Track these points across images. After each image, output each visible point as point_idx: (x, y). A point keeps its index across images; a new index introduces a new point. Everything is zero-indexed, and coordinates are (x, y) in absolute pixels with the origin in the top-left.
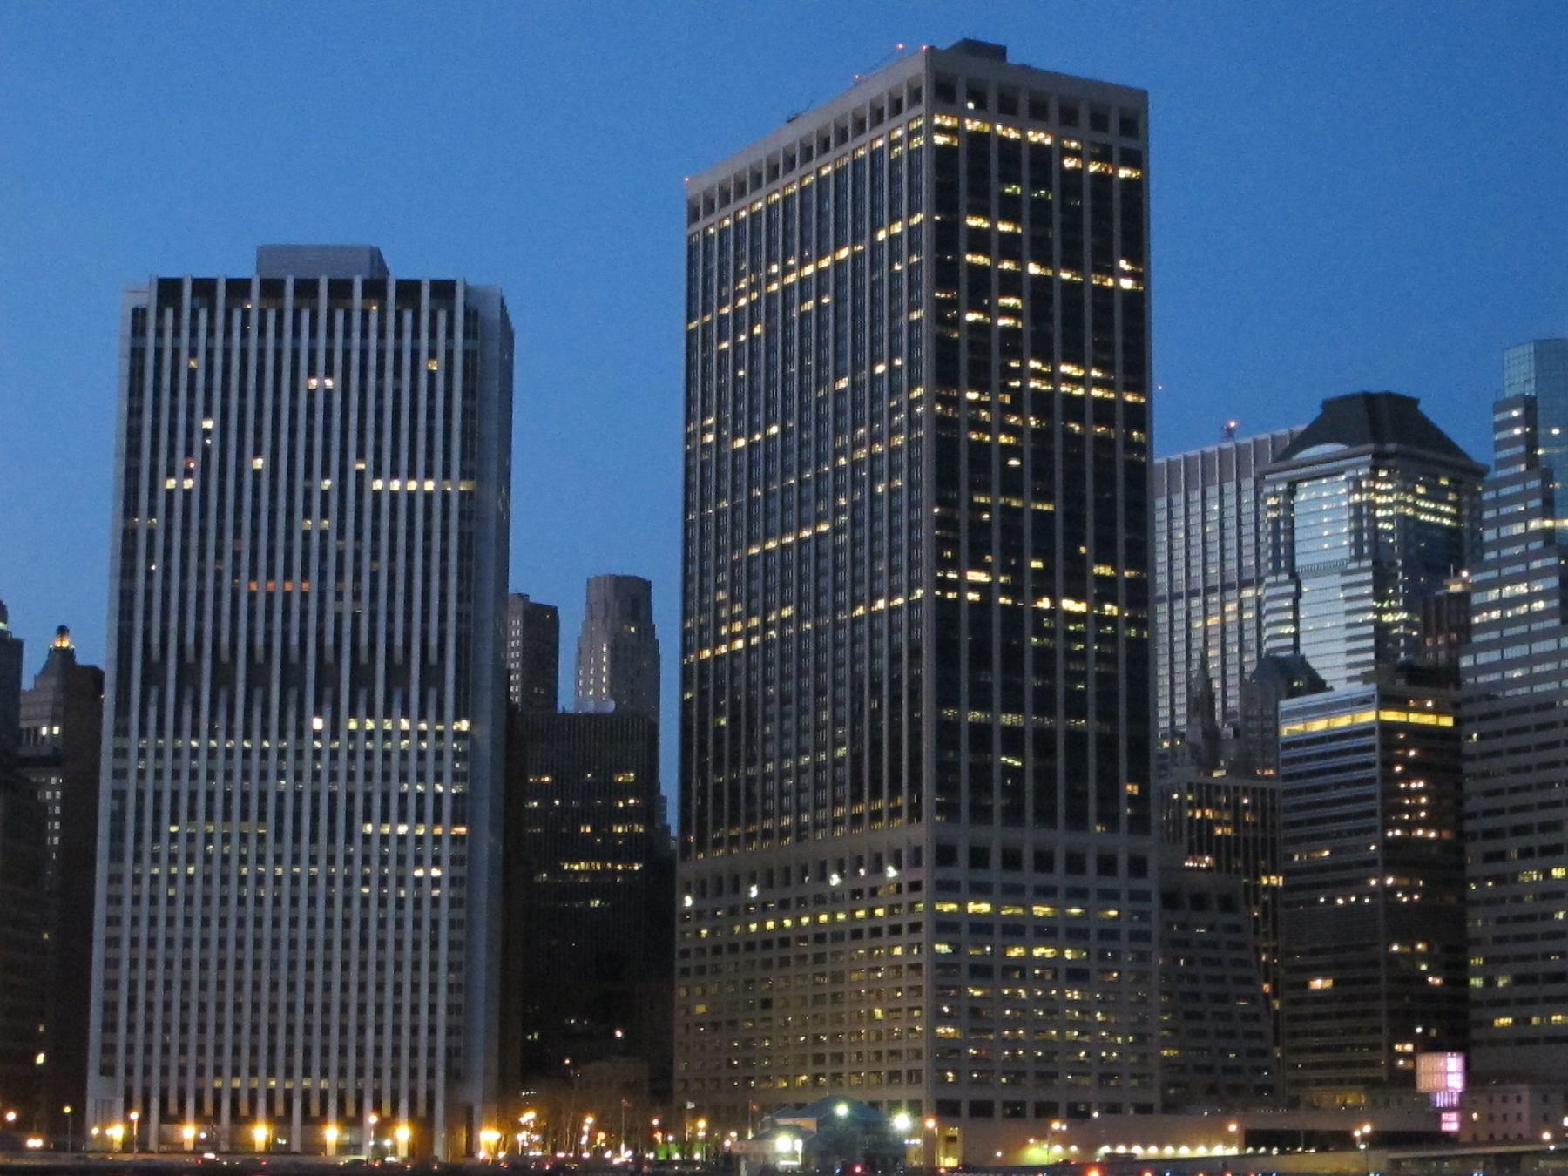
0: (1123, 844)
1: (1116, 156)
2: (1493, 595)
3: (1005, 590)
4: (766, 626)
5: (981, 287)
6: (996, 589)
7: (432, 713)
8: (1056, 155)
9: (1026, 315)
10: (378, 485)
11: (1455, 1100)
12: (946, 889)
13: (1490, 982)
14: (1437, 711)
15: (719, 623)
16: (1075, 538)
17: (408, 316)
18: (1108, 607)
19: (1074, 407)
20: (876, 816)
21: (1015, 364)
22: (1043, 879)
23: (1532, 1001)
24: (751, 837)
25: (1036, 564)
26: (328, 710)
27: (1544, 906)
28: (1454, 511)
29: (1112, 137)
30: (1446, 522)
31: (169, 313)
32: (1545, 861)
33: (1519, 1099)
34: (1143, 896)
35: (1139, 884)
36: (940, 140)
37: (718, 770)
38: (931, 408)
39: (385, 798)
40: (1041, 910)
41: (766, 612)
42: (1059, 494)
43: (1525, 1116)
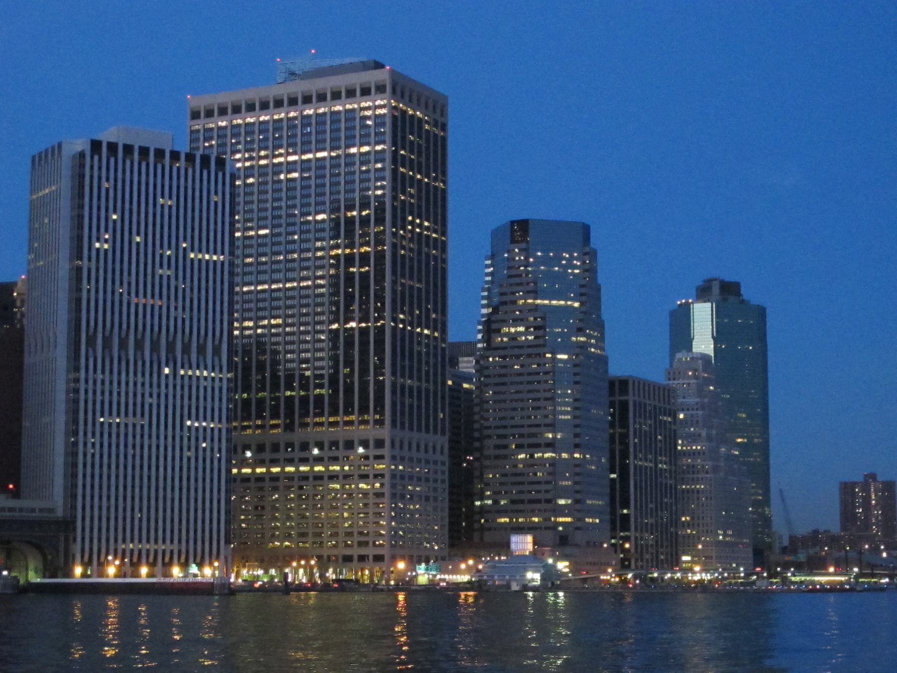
7: (217, 369)
10: (192, 256)
13: (496, 502)
16: (428, 302)
17: (112, 160)
20: (350, 423)
24: (245, 428)
26: (171, 364)
29: (437, 116)
31: (96, 158)
32: (531, 450)
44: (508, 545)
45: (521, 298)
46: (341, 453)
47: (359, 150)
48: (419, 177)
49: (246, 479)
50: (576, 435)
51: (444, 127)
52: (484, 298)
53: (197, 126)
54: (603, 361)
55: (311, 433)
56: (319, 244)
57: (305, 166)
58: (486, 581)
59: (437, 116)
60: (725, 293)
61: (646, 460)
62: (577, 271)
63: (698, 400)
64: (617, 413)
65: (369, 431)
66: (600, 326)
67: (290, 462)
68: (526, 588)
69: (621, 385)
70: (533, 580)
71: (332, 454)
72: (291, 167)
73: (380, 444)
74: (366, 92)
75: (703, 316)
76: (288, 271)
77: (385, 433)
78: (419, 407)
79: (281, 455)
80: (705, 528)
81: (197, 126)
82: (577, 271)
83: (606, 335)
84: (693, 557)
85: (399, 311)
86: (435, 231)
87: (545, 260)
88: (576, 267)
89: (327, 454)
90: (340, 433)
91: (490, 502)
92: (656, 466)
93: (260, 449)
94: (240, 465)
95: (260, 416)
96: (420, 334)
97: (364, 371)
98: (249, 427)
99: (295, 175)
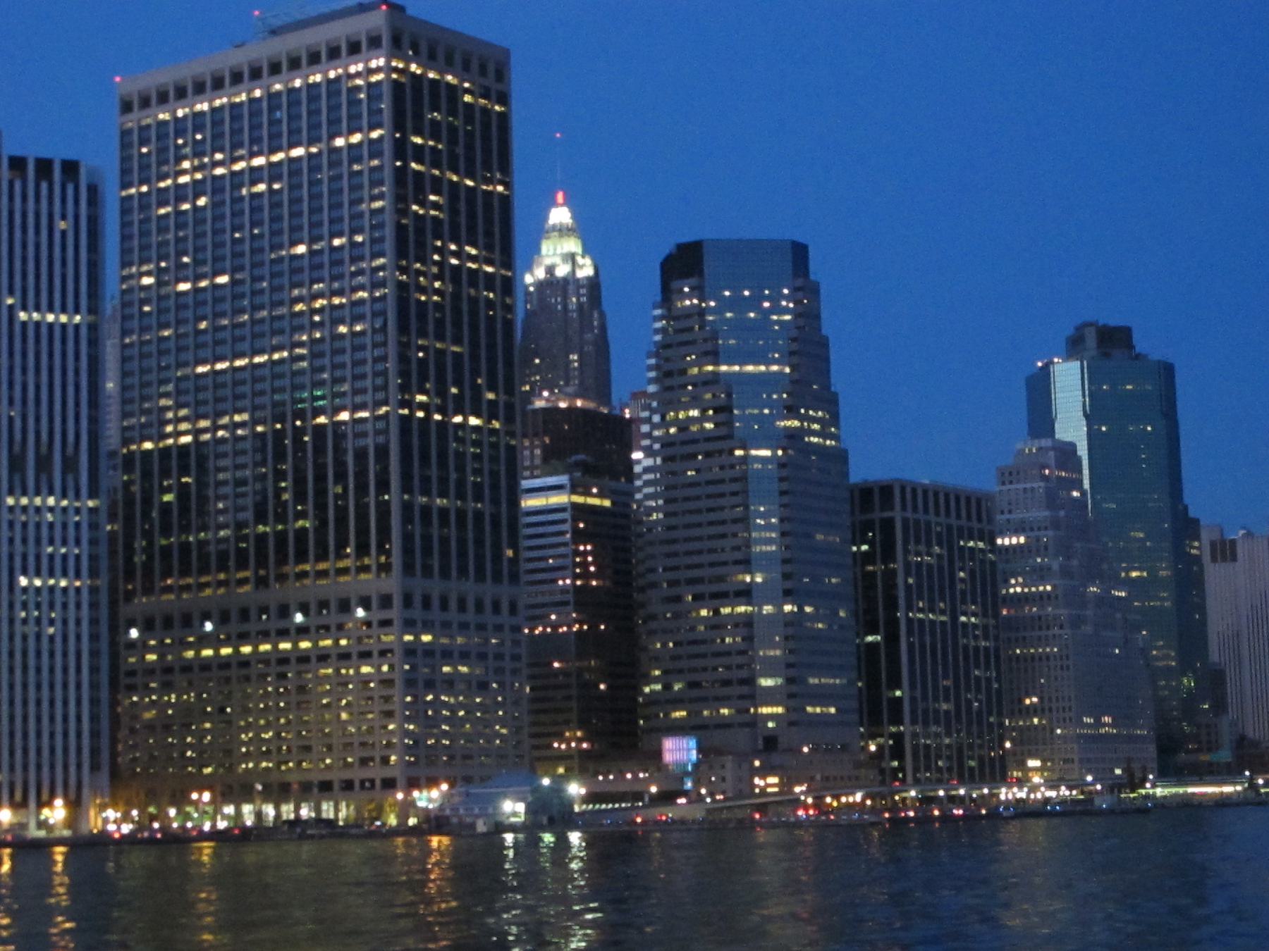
1: (494, 96)
4: (216, 428)
6: (432, 408)
8: (460, 92)
9: (446, 208)
10: (23, 316)
12: (409, 625)
13: (667, 687)
14: (600, 495)
16: (475, 373)
20: (345, 571)
21: (439, 243)
24: (202, 586)
25: (454, 390)
29: (490, 81)
32: (717, 602)
33: (723, 767)
36: (394, 76)
37: (166, 532)
39: (38, 557)
40: (426, 638)
42: (466, 340)
44: (658, 754)
45: (693, 364)
46: (332, 618)
48: (470, 183)
49: (205, 665)
50: (786, 576)
51: (503, 99)
52: (650, 368)
53: (131, 122)
54: (840, 457)
55: (293, 591)
56: (296, 292)
57: (273, 172)
58: (447, 818)
59: (490, 81)
60: (1106, 345)
61: (932, 611)
62: (788, 317)
64: (878, 539)
66: (829, 402)
67: (265, 636)
68: (501, 827)
69: (872, 497)
70: (515, 814)
71: (321, 621)
72: (255, 175)
73: (386, 601)
74: (354, 49)
75: (1068, 381)
77: (392, 584)
78: (462, 542)
79: (252, 627)
81: (131, 122)
82: (788, 317)
83: (842, 415)
84: (1044, 761)
85: (414, 389)
86: (490, 262)
87: (737, 304)
88: (786, 311)
89: (315, 621)
91: (658, 687)
92: (954, 618)
93: (223, 619)
94: (198, 646)
95: (223, 567)
96: (463, 426)
97: (362, 488)
98: (207, 585)
99: (261, 187)
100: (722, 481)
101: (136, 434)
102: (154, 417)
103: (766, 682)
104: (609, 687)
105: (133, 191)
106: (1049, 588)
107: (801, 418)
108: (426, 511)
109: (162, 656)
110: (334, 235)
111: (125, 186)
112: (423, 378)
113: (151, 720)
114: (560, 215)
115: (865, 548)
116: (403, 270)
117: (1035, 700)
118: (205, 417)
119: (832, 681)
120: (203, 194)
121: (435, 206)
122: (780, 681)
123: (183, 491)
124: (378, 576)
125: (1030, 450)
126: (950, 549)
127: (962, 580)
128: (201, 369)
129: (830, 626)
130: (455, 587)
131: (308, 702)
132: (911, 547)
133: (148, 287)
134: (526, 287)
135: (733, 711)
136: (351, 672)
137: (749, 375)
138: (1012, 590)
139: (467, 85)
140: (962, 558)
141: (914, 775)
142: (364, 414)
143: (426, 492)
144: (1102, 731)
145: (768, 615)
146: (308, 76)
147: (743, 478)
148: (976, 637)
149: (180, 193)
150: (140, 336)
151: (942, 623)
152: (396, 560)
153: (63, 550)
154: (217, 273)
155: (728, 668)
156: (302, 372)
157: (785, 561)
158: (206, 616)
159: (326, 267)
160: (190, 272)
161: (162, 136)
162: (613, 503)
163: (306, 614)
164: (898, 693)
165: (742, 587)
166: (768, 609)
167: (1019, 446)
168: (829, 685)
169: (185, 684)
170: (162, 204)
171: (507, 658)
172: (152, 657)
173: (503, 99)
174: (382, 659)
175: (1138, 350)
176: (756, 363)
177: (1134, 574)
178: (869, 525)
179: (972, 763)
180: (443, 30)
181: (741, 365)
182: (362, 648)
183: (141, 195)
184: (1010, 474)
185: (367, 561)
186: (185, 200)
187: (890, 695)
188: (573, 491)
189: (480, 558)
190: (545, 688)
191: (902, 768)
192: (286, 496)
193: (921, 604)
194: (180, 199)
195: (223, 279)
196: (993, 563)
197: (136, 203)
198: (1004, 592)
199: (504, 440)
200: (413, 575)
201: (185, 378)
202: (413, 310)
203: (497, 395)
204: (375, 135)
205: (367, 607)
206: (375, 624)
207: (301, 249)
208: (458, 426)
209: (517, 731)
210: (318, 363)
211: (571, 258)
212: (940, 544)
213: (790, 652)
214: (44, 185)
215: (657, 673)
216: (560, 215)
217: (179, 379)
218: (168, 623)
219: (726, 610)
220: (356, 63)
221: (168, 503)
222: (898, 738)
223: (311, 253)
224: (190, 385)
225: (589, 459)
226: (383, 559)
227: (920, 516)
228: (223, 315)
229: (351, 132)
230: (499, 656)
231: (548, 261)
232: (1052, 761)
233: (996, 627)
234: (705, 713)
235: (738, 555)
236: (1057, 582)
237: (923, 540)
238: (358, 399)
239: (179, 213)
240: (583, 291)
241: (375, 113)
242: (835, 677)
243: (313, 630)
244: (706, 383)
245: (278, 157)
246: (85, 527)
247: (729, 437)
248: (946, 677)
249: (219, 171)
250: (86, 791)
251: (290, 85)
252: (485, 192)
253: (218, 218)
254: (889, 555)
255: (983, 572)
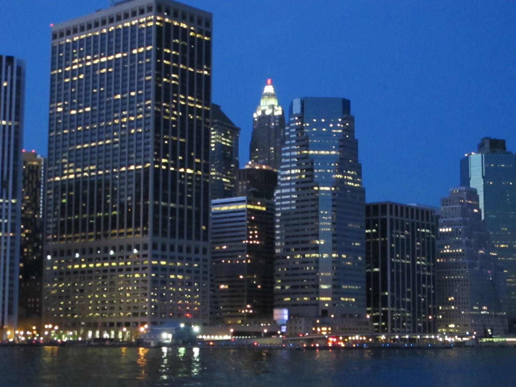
0: (201, 244)
1: (204, 33)
2: (288, 172)
3: (173, 166)
4: (83, 172)
5: (168, 71)
6: (170, 165)
8: (188, 31)
11: (285, 322)
12: (155, 257)
13: (283, 287)
14: (261, 205)
15: (64, 169)
16: (191, 150)
18: (199, 172)
19: (192, 110)
20: (130, 233)
21: (175, 95)
22: (180, 254)
23: (298, 293)
24: (76, 238)
25: (180, 158)
27: (303, 265)
28: (231, 141)
29: (203, 27)
30: (228, 145)
32: (303, 252)
33: (301, 322)
34: (205, 260)
35: (205, 257)
36: (158, 23)
38: (153, 108)
40: (163, 263)
41: (84, 166)
43: (303, 327)
46: (124, 253)
47: (138, 51)
49: (76, 272)
50: (334, 242)
53: (56, 42)
54: (361, 191)
60: (494, 147)
61: (403, 259)
62: (340, 131)
63: (461, 219)
64: (380, 226)
65: (140, 238)
66: (357, 167)
67: (99, 260)
68: (161, 345)
70: (168, 339)
71: (120, 254)
72: (102, 65)
73: (145, 247)
75: (476, 161)
76: (100, 134)
77: (148, 239)
78: (181, 223)
79: (94, 256)
80: (464, 305)
81: (56, 42)
82: (340, 131)
84: (456, 325)
87: (319, 125)
90: (124, 240)
92: (414, 262)
93: (83, 253)
95: (84, 230)
99: (104, 70)
100: (307, 200)
101: (53, 174)
102: (60, 167)
103: (324, 287)
104: (262, 287)
105: (56, 72)
106: (461, 250)
107: (343, 175)
108: (165, 209)
109: (59, 267)
110: (131, 91)
111: (53, 70)
112: (166, 151)
113: (54, 294)
114: (269, 89)
115: (374, 230)
116: (159, 106)
117: (453, 298)
118: (79, 167)
119: (354, 287)
120: (82, 73)
121: (174, 79)
122: (330, 286)
123: (70, 198)
124: (143, 235)
125: (456, 192)
126: (413, 233)
127: (418, 246)
128: (79, 147)
129: (354, 264)
130: (177, 242)
131: (114, 288)
132: (394, 231)
133: (60, 112)
134: (254, 119)
135: (309, 299)
136: (131, 276)
137: (322, 155)
138: (445, 251)
139: (192, 28)
140: (418, 237)
141: (392, 329)
142: (140, 167)
143: (165, 200)
144: (483, 313)
145: (326, 258)
146: (123, 24)
147: (317, 199)
148: (424, 271)
149: (73, 73)
150: (56, 132)
151: (408, 264)
152: (150, 229)
153: (6, 221)
154: (86, 106)
155: (308, 280)
156: (116, 149)
157: (334, 235)
158: (77, 251)
159: (129, 104)
160: (76, 106)
161: (67, 49)
162: (267, 209)
163: (115, 251)
164: (387, 293)
165: (315, 246)
166: (325, 256)
167: (451, 189)
168: (351, 289)
169: (68, 279)
170: (66, 77)
171: (201, 272)
172: (55, 268)
173: (208, 34)
174: (143, 272)
175: (508, 150)
176: (326, 150)
177: (502, 246)
178: (376, 221)
179: (420, 325)
180: (192, 8)
181: (318, 151)
182: (136, 266)
183: (59, 74)
184: (447, 201)
185: (139, 229)
186: (75, 76)
187: (383, 294)
188: (249, 202)
189: (190, 230)
190: (235, 286)
191: (386, 326)
192: (109, 201)
193: (398, 256)
194: (73, 75)
195: (88, 109)
196: (433, 239)
197: (56, 77)
198: (442, 252)
199: (203, 180)
200: (175, 237)
201: (72, 150)
202: (162, 122)
203: (200, 160)
204: (149, 48)
205: (138, 249)
206: (141, 256)
207: (119, 96)
208: (182, 173)
209: (203, 303)
210: (123, 145)
211: (272, 107)
212: (408, 230)
213: (335, 274)
214: (9, 68)
215: (279, 281)
216: (269, 89)
217: (70, 151)
218: (62, 254)
219: (307, 256)
220: (143, 18)
221: (64, 203)
222: (385, 312)
223: (122, 98)
224: (74, 153)
225: (257, 190)
226: (145, 228)
227: (399, 218)
228: (87, 124)
229: (139, 47)
230: (197, 272)
231: (263, 108)
232: (459, 325)
233: (434, 266)
234: (298, 299)
235: (313, 232)
236: (464, 248)
237: (400, 228)
238: (138, 160)
239: (72, 81)
240: (277, 121)
241: (149, 39)
242: (355, 286)
243: (117, 258)
244: (303, 158)
245: (111, 58)
246: (10, 211)
247: (312, 181)
248: (409, 287)
249: (89, 64)
250: (6, 322)
251: (117, 27)
252: (198, 74)
253: (87, 83)
254: (384, 235)
255: (428, 243)
